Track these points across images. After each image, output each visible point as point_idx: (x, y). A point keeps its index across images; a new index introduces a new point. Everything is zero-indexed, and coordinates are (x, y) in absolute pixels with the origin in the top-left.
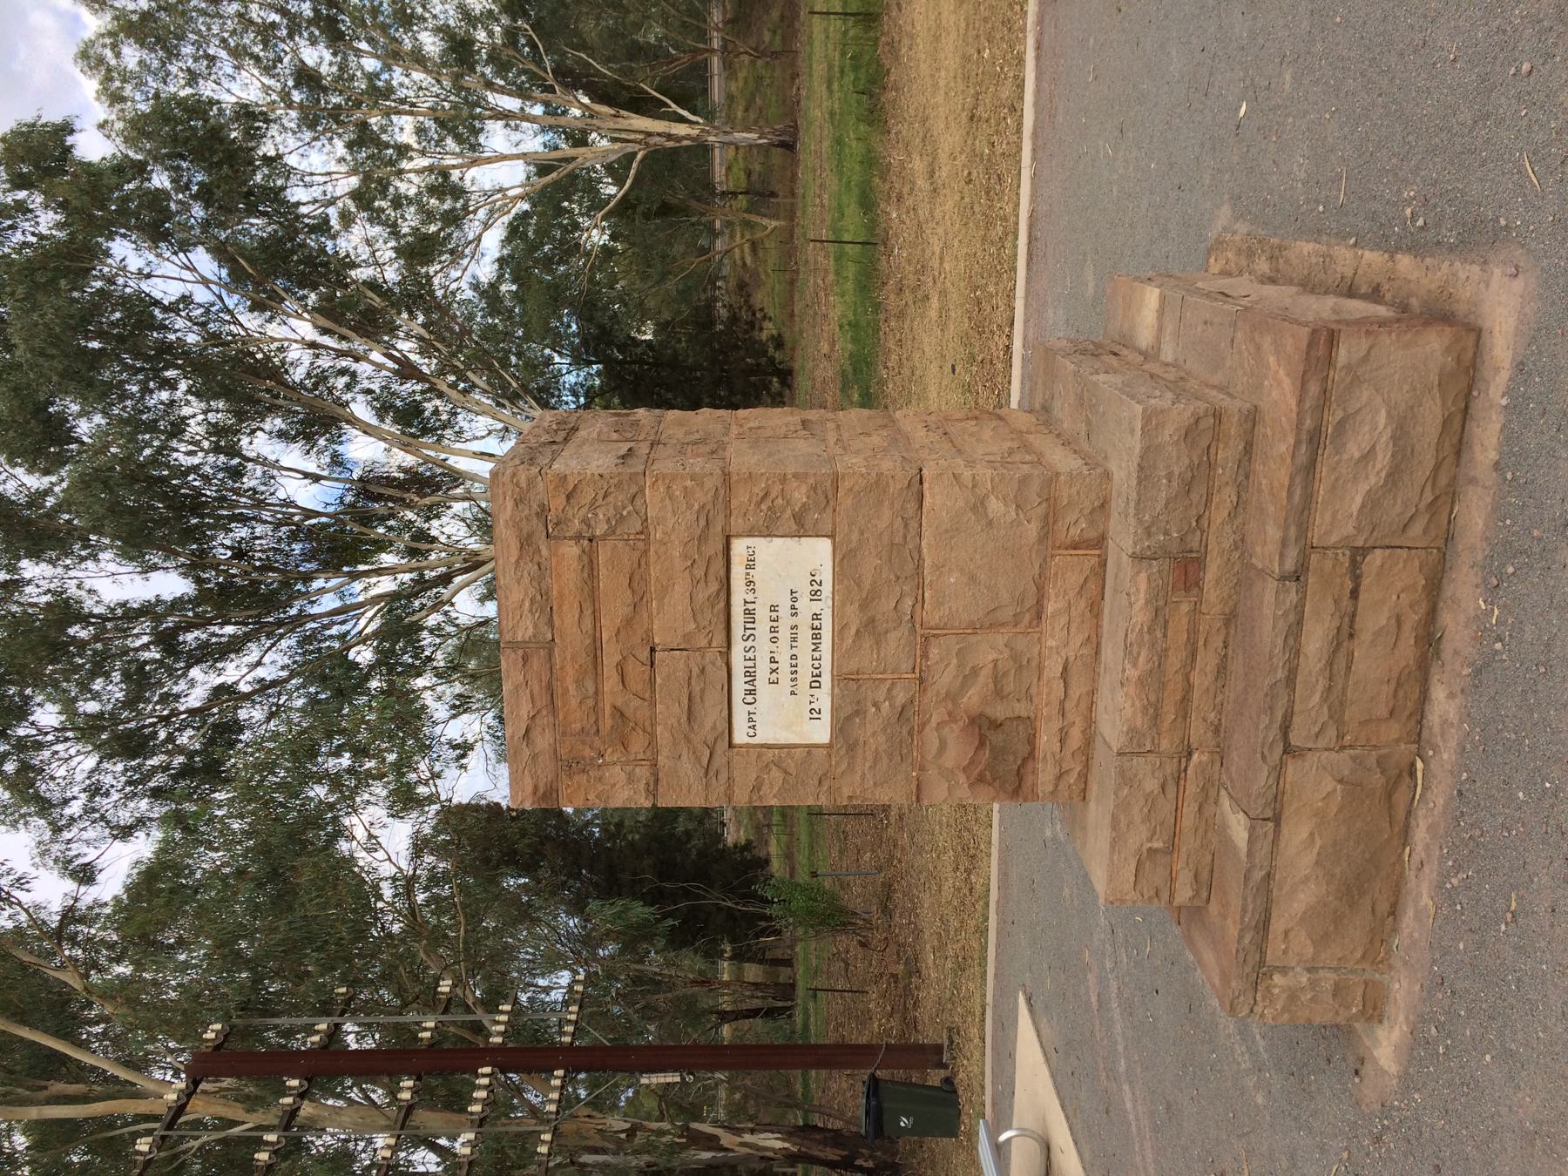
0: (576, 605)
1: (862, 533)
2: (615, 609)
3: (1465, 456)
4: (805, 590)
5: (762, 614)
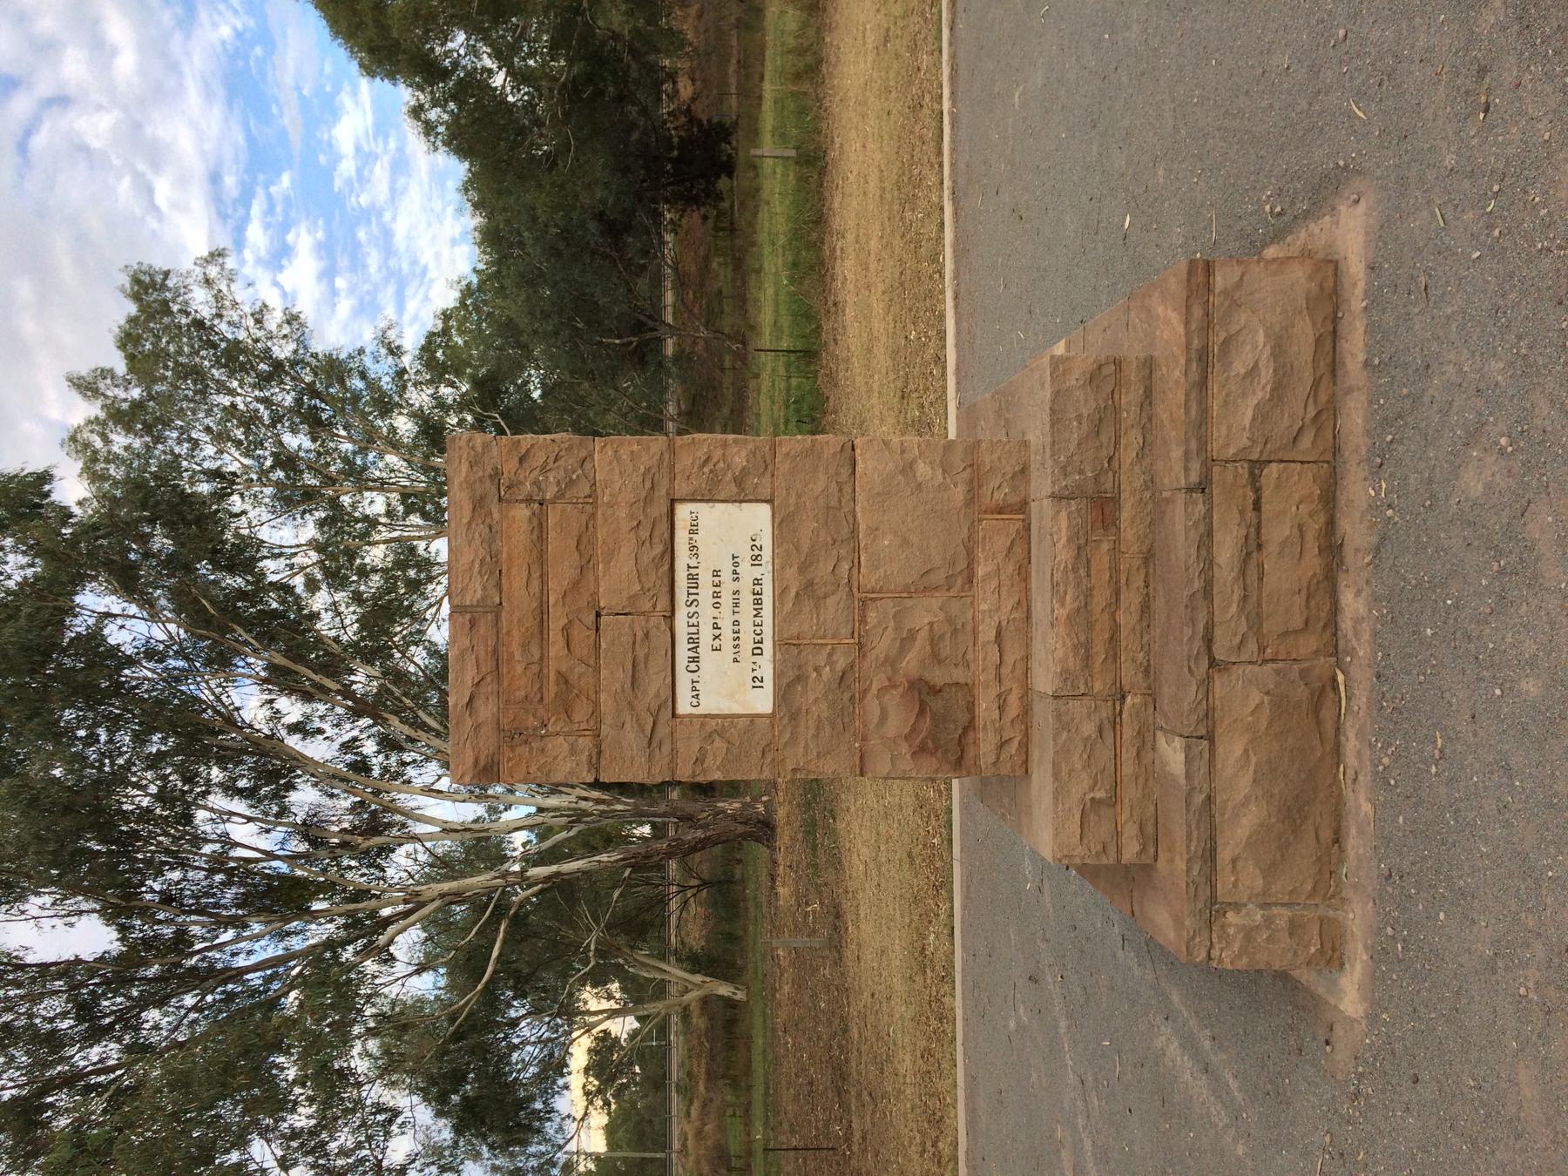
0: (525, 566)
1: (799, 496)
2: (562, 573)
3: (1340, 373)
4: (746, 554)
5: (705, 579)
